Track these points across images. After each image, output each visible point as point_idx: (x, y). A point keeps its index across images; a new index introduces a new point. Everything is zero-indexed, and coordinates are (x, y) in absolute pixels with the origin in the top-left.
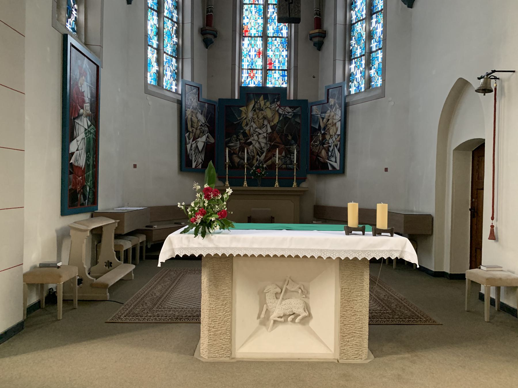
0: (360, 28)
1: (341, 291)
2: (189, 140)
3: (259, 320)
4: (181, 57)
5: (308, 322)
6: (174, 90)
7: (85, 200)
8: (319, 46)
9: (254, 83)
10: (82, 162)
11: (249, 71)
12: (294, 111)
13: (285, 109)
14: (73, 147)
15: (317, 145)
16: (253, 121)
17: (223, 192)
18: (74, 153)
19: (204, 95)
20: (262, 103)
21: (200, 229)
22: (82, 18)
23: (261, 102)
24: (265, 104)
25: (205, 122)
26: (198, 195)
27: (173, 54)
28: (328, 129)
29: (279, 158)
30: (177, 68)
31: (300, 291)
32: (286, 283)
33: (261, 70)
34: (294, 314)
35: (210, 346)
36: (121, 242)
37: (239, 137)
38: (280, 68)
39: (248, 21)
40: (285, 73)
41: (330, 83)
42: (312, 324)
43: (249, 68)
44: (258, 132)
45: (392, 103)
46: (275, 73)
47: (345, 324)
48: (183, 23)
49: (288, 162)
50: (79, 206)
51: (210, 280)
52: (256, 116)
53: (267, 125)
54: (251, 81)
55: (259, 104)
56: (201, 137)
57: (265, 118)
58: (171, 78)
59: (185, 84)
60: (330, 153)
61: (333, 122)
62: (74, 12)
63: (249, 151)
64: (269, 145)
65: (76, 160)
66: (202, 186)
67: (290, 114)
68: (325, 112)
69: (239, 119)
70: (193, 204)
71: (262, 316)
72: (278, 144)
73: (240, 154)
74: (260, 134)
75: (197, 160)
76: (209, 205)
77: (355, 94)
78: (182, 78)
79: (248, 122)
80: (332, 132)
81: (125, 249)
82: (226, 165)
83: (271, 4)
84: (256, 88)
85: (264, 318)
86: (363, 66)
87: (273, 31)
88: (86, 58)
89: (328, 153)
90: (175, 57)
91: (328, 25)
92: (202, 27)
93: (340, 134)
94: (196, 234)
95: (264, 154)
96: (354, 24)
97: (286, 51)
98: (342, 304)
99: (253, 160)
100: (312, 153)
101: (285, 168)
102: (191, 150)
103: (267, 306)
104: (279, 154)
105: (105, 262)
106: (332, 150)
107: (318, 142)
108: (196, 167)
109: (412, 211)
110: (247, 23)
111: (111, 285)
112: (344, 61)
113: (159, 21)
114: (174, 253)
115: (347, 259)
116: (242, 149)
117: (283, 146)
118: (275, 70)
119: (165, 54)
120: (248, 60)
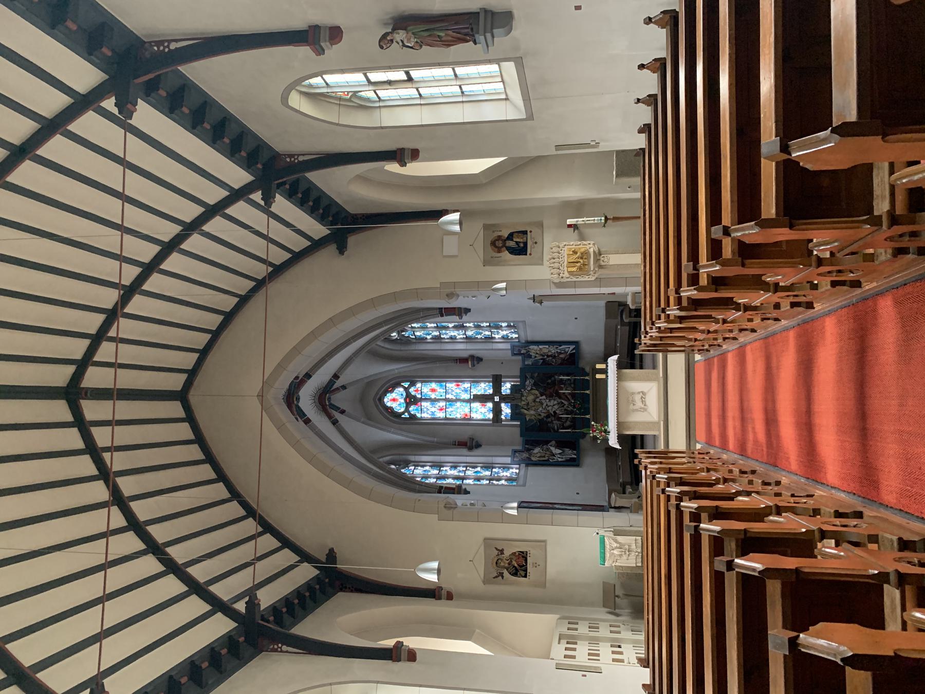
0: (469, 333)
2: (554, 459)
6: (517, 471)
8: (480, 360)
17: (593, 425)
19: (519, 448)
20: (523, 403)
24: (524, 401)
29: (566, 390)
30: (499, 468)
41: (510, 352)
48: (466, 463)
49: (569, 382)
52: (533, 408)
57: (534, 401)
60: (562, 352)
63: (561, 413)
69: (535, 422)
71: (642, 410)
74: (547, 405)
75: (570, 454)
80: (546, 351)
82: (573, 432)
90: (492, 469)
91: (465, 355)
95: (563, 401)
96: (466, 336)
98: (637, 380)
100: (561, 364)
102: (562, 458)
108: (575, 455)
112: (493, 342)
116: (559, 419)
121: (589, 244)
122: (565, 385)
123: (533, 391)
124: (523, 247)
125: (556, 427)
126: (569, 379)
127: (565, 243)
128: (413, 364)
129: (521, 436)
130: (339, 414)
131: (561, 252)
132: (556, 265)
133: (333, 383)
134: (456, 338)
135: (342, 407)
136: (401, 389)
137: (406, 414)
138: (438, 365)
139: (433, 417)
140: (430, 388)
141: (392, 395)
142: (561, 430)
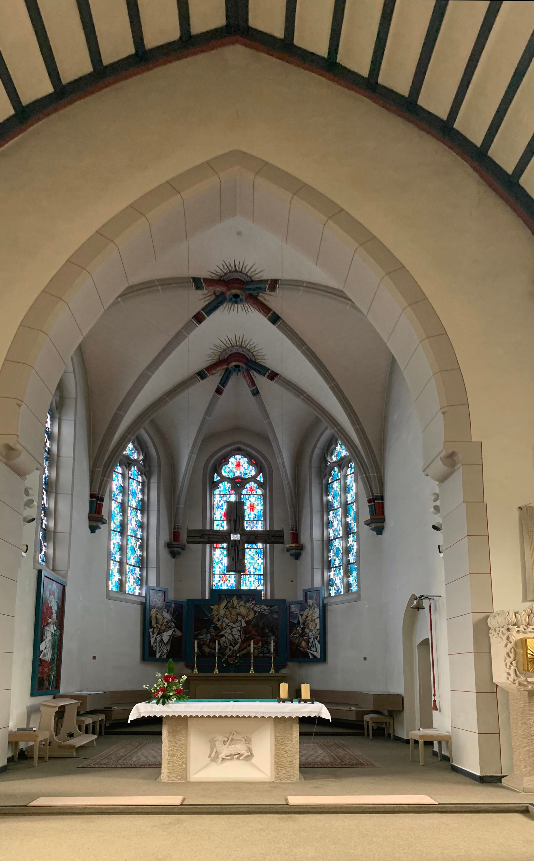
0: (338, 544)
1: (275, 738)
2: (153, 634)
3: (209, 759)
4: (145, 566)
5: (251, 759)
6: (137, 594)
7: (49, 685)
8: (297, 556)
9: (227, 586)
10: (48, 658)
14: (42, 647)
15: (297, 637)
17: (180, 677)
18: (43, 651)
19: (171, 596)
20: (236, 602)
21: (161, 701)
22: (51, 552)
24: (238, 603)
25: (172, 619)
26: (159, 680)
27: (136, 564)
28: (308, 624)
29: (254, 648)
30: (141, 575)
31: (243, 740)
32: (232, 734)
34: (239, 754)
35: (169, 773)
36: (83, 718)
40: (261, 577)
42: (254, 760)
45: (368, 606)
47: (279, 759)
50: (45, 690)
51: (169, 732)
52: (228, 613)
53: (241, 620)
56: (166, 632)
57: (238, 614)
58: (134, 584)
59: (149, 589)
60: (310, 644)
61: (312, 619)
62: (44, 548)
63: (221, 642)
65: (44, 656)
66: (163, 674)
67: (267, 611)
68: (304, 610)
70: (155, 686)
71: (213, 755)
73: (211, 645)
74: (233, 628)
75: (161, 651)
76: (168, 686)
77: (335, 596)
78: (147, 584)
81: (86, 724)
82: (194, 655)
85: (214, 757)
86: (342, 574)
88: (55, 582)
89: (308, 644)
90: (138, 567)
91: (304, 539)
92: (168, 541)
93: (319, 628)
94: (158, 703)
95: (239, 645)
100: (292, 643)
102: (155, 642)
103: (217, 749)
104: (254, 644)
105: (67, 733)
106: (313, 642)
107: (298, 635)
108: (160, 657)
109: (389, 692)
111: (77, 746)
113: (122, 540)
114: (140, 715)
115: (277, 717)
116: (213, 641)
117: (259, 638)
118: (250, 575)
119: (128, 566)
122: (262, 647)
126: (270, 651)
128: (291, 484)
129: (188, 600)
130: (216, 387)
133: (263, 371)
134: (328, 527)
135: (226, 390)
136: (253, 473)
137: (219, 478)
138: (289, 509)
139: (215, 506)
140: (256, 504)
141: (246, 463)
142: (196, 642)
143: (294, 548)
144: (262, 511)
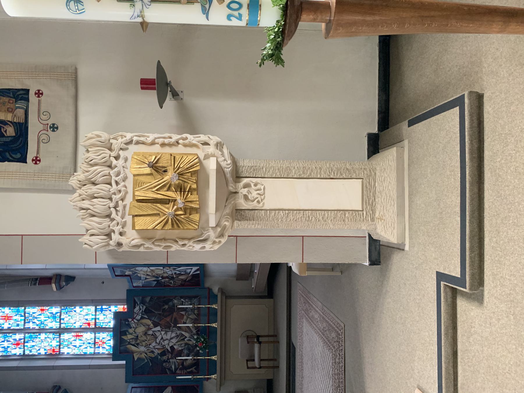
8: (70, 279)
9: (110, 340)
11: (96, 347)
12: (139, 303)
13: (136, 313)
16: (148, 346)
20: (130, 337)
23: (129, 338)
24: (131, 334)
28: (157, 275)
33: (95, 334)
37: (165, 360)
38: (94, 313)
39: (43, 349)
43: (93, 347)
44: (161, 340)
46: (98, 319)
52: (144, 343)
53: (153, 331)
54: (107, 344)
55: (131, 340)
57: (146, 334)
60: (182, 273)
64: (173, 329)
67: (141, 307)
69: (146, 361)
72: (173, 319)
74: (162, 338)
79: (150, 351)
83: (24, 325)
84: (115, 337)
87: (54, 322)
95: (183, 333)
97: (75, 308)
99: (189, 344)
100: (182, 285)
101: (198, 311)
106: (179, 271)
110: (45, 350)
118: (95, 319)
120: (84, 348)
121: (206, 144)
123: (144, 321)
124: (15, 139)
125: (173, 367)
127: (129, 136)
131: (114, 162)
132: (99, 205)
139: (4, 354)
143: (57, 284)
144: (12, 308)
